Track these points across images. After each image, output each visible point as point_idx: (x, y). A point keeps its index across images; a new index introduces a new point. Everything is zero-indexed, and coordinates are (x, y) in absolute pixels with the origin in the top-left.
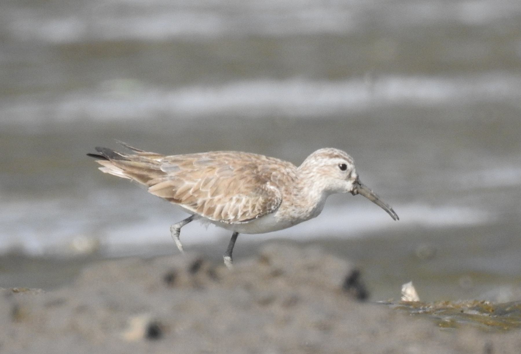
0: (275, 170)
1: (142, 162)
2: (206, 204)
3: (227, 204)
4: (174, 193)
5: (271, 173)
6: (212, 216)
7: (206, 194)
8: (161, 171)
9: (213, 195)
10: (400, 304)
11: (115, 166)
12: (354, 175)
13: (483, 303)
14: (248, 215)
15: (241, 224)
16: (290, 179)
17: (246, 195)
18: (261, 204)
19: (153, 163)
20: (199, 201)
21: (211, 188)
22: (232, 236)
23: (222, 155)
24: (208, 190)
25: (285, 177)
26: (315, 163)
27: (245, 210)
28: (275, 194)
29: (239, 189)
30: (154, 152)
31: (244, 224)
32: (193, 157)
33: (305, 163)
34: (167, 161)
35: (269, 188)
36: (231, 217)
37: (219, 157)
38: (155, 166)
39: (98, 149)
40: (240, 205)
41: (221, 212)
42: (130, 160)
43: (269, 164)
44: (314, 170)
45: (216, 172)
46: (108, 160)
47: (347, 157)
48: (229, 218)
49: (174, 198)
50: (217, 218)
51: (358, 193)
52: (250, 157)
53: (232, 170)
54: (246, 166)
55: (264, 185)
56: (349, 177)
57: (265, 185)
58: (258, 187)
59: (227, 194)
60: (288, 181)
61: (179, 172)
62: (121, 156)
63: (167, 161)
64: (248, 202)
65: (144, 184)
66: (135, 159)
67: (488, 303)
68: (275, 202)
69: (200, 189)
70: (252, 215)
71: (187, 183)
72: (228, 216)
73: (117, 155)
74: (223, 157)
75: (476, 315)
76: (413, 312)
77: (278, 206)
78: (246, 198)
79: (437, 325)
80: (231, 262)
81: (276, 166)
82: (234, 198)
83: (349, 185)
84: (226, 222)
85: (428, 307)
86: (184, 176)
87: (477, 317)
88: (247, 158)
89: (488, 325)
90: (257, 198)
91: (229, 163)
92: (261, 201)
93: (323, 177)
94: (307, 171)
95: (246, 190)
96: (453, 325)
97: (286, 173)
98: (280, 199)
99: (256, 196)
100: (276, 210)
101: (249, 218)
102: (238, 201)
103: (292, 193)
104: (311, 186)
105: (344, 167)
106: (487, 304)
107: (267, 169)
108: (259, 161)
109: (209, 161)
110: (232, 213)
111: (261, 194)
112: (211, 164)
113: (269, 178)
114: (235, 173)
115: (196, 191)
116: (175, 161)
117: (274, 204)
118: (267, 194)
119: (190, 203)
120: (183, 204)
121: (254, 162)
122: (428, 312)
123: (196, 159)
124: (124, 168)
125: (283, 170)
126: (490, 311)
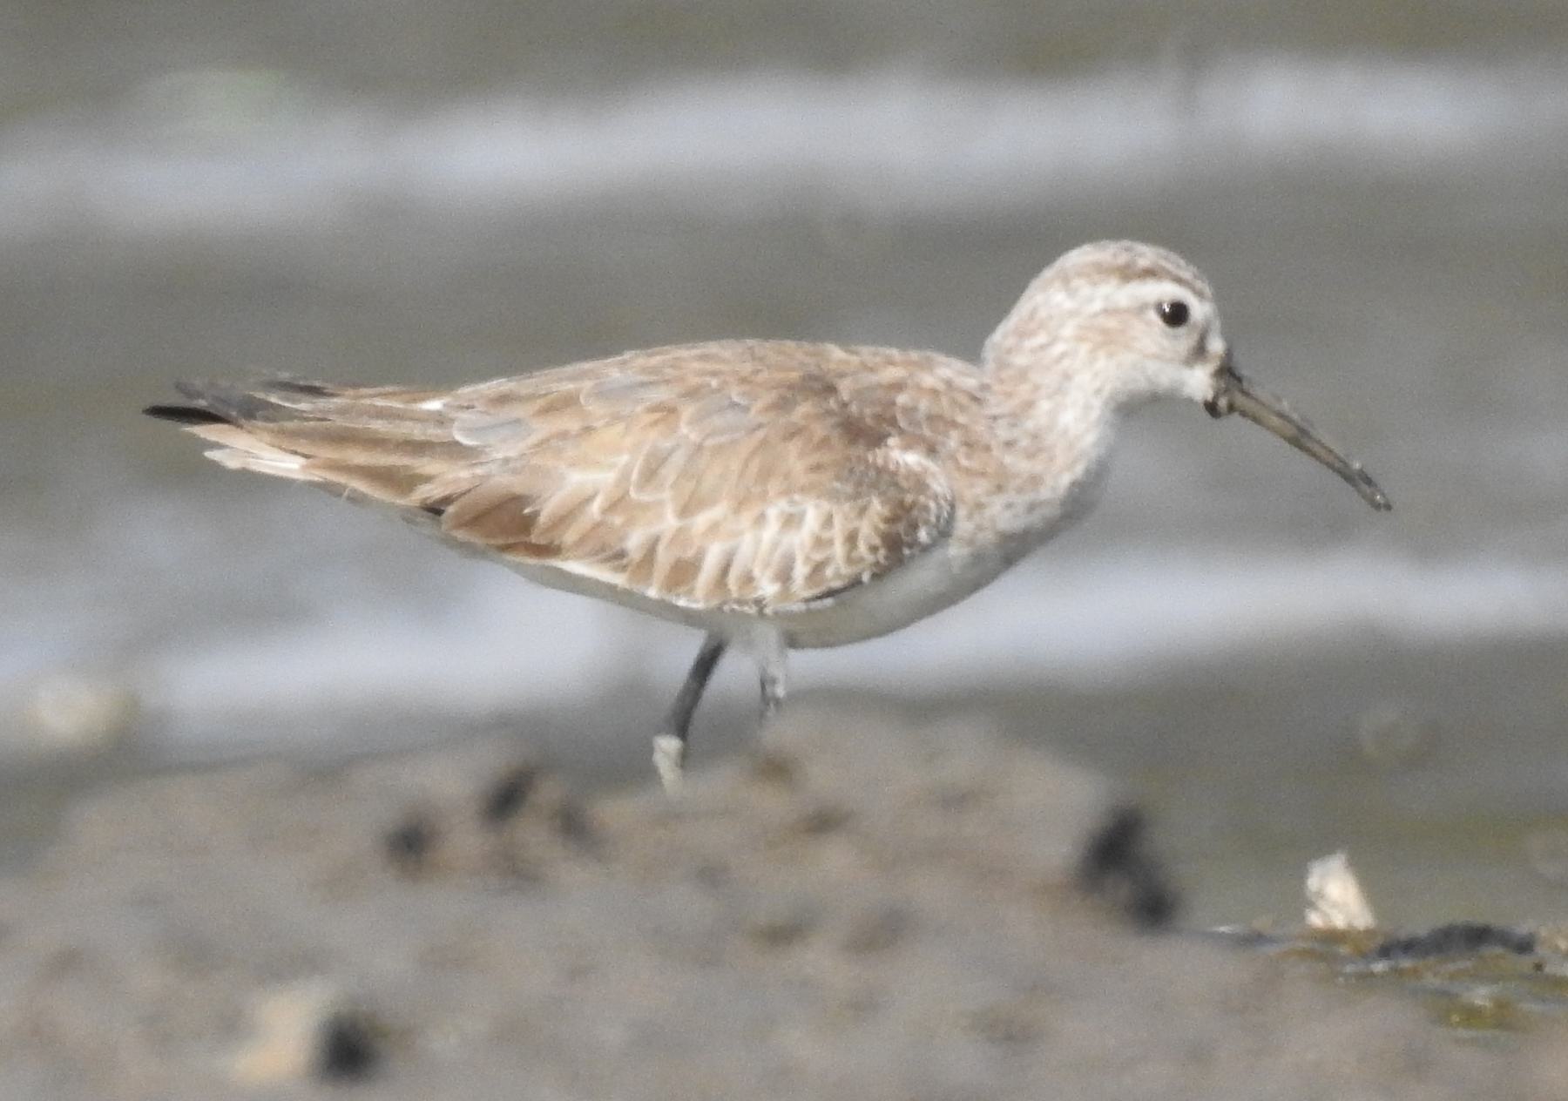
0: (898, 386)
2: (661, 549)
5: (893, 403)
8: (457, 443)
9: (686, 511)
11: (267, 444)
12: (1216, 346)
15: (809, 611)
17: (819, 497)
20: (634, 542)
21: (674, 485)
24: (666, 497)
27: (818, 557)
29: (787, 476)
31: (819, 611)
32: (572, 379)
35: (901, 462)
36: (768, 588)
40: (800, 539)
48: (760, 593)
50: (707, 597)
51: (1231, 408)
54: (791, 387)
56: (1199, 352)
59: (740, 505)
61: (534, 439)
62: (280, 406)
63: (473, 407)
64: (828, 522)
65: (401, 501)
69: (633, 494)
70: (846, 570)
72: (755, 584)
74: (696, 365)
76: (1349, 969)
78: (817, 506)
79: (1442, 1018)
82: (774, 512)
83: (1199, 382)
84: (746, 608)
90: (860, 502)
93: (1101, 354)
94: (1041, 338)
95: (814, 477)
96: (1502, 1018)
101: (837, 584)
102: (791, 521)
103: (993, 443)
104: (1059, 391)
105: (1176, 315)
109: (643, 385)
110: (769, 573)
111: (874, 486)
113: (893, 422)
114: (762, 419)
116: (503, 400)
117: (927, 522)
118: (896, 485)
119: (596, 553)
123: (588, 385)
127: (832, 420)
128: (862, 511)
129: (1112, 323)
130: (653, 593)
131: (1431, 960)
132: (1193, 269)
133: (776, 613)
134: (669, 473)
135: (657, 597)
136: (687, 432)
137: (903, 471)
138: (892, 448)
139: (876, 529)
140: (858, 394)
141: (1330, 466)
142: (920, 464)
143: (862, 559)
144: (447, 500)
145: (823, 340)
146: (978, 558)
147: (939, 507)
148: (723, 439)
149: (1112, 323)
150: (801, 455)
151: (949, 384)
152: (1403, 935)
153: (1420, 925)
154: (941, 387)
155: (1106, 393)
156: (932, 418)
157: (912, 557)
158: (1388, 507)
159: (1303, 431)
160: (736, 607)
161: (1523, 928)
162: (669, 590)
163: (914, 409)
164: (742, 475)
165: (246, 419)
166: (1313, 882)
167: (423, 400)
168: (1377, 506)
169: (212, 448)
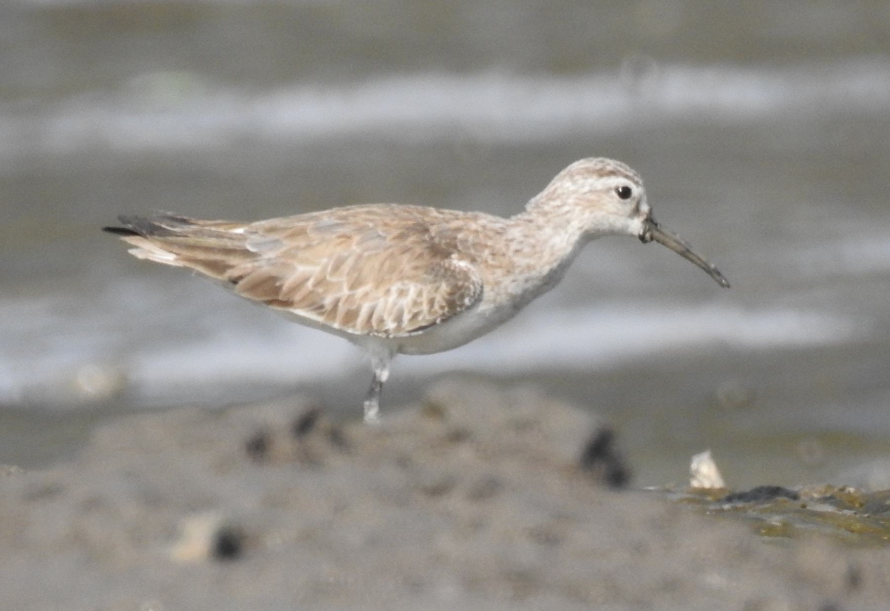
0: (459, 230)
2: (340, 304)
3: (382, 301)
5: (455, 238)
6: (354, 326)
7: (339, 285)
9: (353, 287)
10: (691, 493)
12: (645, 208)
13: (842, 490)
15: (410, 336)
18: (447, 297)
19: (231, 238)
20: (328, 301)
21: (348, 274)
23: (360, 213)
24: (342, 280)
26: (572, 188)
27: (415, 310)
28: (470, 276)
29: (401, 272)
33: (550, 188)
35: (457, 265)
36: (391, 325)
37: (354, 216)
39: (121, 219)
40: (406, 302)
42: (187, 236)
43: (447, 222)
44: (571, 201)
47: (631, 174)
49: (281, 298)
50: (362, 329)
51: (652, 238)
54: (407, 229)
55: (446, 260)
56: (637, 211)
58: (437, 264)
59: (379, 283)
61: (284, 249)
64: (420, 294)
65: (220, 277)
66: (195, 233)
67: (852, 490)
69: (328, 278)
70: (429, 318)
71: (301, 269)
73: (161, 228)
74: (363, 216)
75: (830, 513)
76: (712, 507)
79: (757, 531)
82: (395, 288)
83: (636, 226)
84: (380, 335)
86: (294, 257)
87: (832, 516)
89: (852, 531)
90: (437, 284)
91: (376, 226)
92: (445, 291)
94: (558, 202)
95: (414, 272)
96: (786, 531)
98: (478, 284)
99: (435, 281)
101: (424, 324)
102: (402, 293)
105: (625, 193)
106: (849, 491)
108: (427, 219)
109: (337, 225)
110: (391, 318)
111: (444, 276)
112: (342, 230)
113: (455, 247)
115: (320, 282)
116: (271, 230)
117: (468, 295)
120: (296, 308)
123: (311, 224)
126: (857, 505)
129: (593, 197)
130: (336, 325)
131: (752, 503)
132: (633, 171)
133: (395, 338)
134: (346, 267)
135: (339, 328)
136: (355, 248)
137: (457, 270)
138: (453, 259)
140: (440, 233)
141: (699, 266)
142: (466, 267)
143: (436, 312)
144: (241, 278)
145: (429, 205)
146: (499, 309)
147: (475, 288)
148: (370, 253)
149: (593, 197)
151: (484, 227)
152: (738, 491)
153: (746, 487)
154: (480, 229)
155: (583, 230)
156: (475, 245)
157: (461, 312)
158: (728, 286)
159: (688, 251)
160: (376, 334)
161: (795, 489)
162: (344, 325)
163: (466, 241)
164: (380, 270)
165: (149, 234)
166: (694, 466)
167: (235, 228)
168: (722, 285)
169: (133, 248)
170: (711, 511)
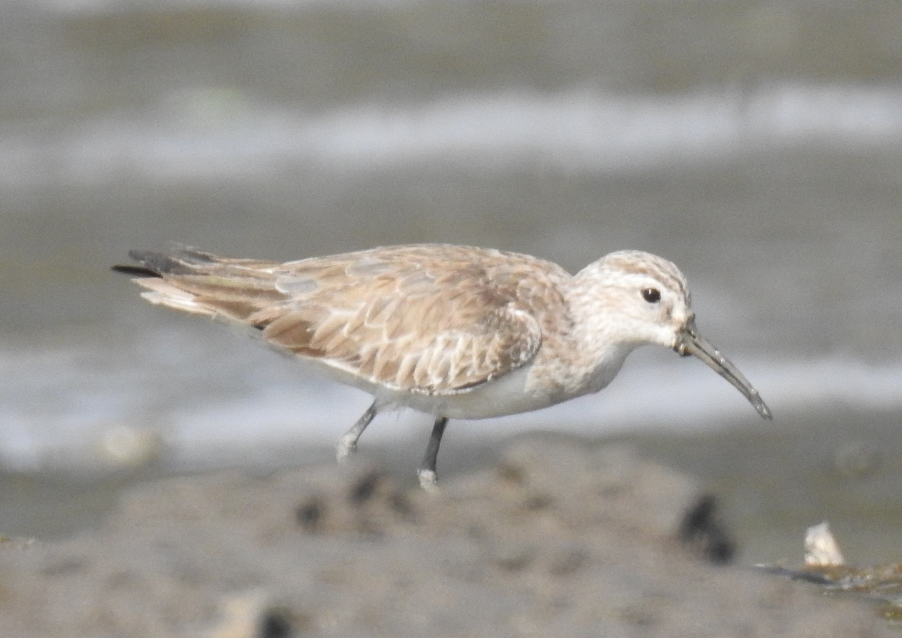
0: (524, 275)
1: (235, 275)
2: (378, 355)
4: (308, 337)
5: (516, 284)
6: (393, 381)
9: (393, 335)
14: (471, 375)
16: (557, 298)
18: (499, 350)
20: (365, 351)
21: (389, 320)
22: (434, 428)
23: (408, 253)
24: (382, 327)
25: (547, 292)
27: (463, 364)
28: (527, 326)
29: (449, 320)
30: (250, 258)
32: (342, 259)
34: (289, 272)
35: (513, 316)
36: (435, 381)
38: (263, 283)
39: (134, 255)
40: (453, 355)
41: (412, 370)
42: (206, 274)
45: (397, 287)
46: (159, 276)
48: (431, 383)
50: (404, 382)
52: (465, 253)
53: (432, 281)
57: (505, 308)
59: (422, 334)
60: (554, 301)
61: (317, 291)
63: (289, 272)
64: (469, 346)
65: (243, 322)
66: (217, 272)
68: (527, 344)
69: (366, 324)
71: (336, 314)
74: (411, 256)
77: (535, 353)
79: (882, 614)
80: (436, 481)
81: (527, 268)
82: (440, 339)
83: (667, 335)
84: (423, 391)
85: (862, 578)
88: (459, 256)
90: (489, 336)
97: (549, 285)
99: (486, 332)
100: (530, 362)
101: (473, 380)
102: (449, 344)
105: (652, 296)
107: (508, 274)
108: (486, 260)
109: (380, 265)
110: (437, 372)
111: (497, 327)
112: (384, 271)
113: (513, 294)
115: (357, 329)
116: (304, 270)
117: (525, 349)
121: (476, 262)
122: (861, 588)
123: (350, 264)
124: (197, 291)
125: (543, 278)
127: (477, 291)
128: (489, 341)
130: (373, 379)
134: (387, 313)
137: (513, 320)
139: (496, 351)
142: (524, 317)
143: (487, 368)
144: (267, 322)
150: (459, 308)
166: (809, 539)
170: (830, 591)
